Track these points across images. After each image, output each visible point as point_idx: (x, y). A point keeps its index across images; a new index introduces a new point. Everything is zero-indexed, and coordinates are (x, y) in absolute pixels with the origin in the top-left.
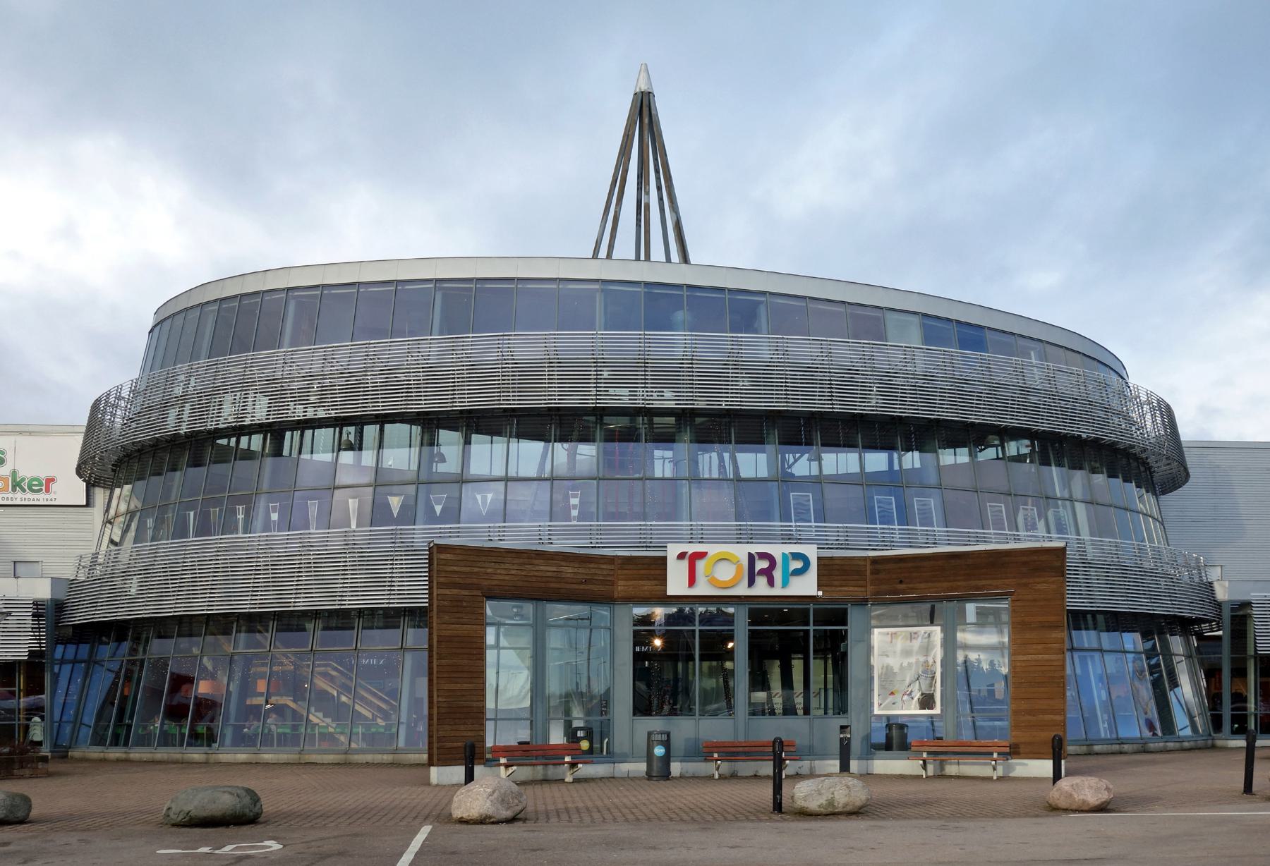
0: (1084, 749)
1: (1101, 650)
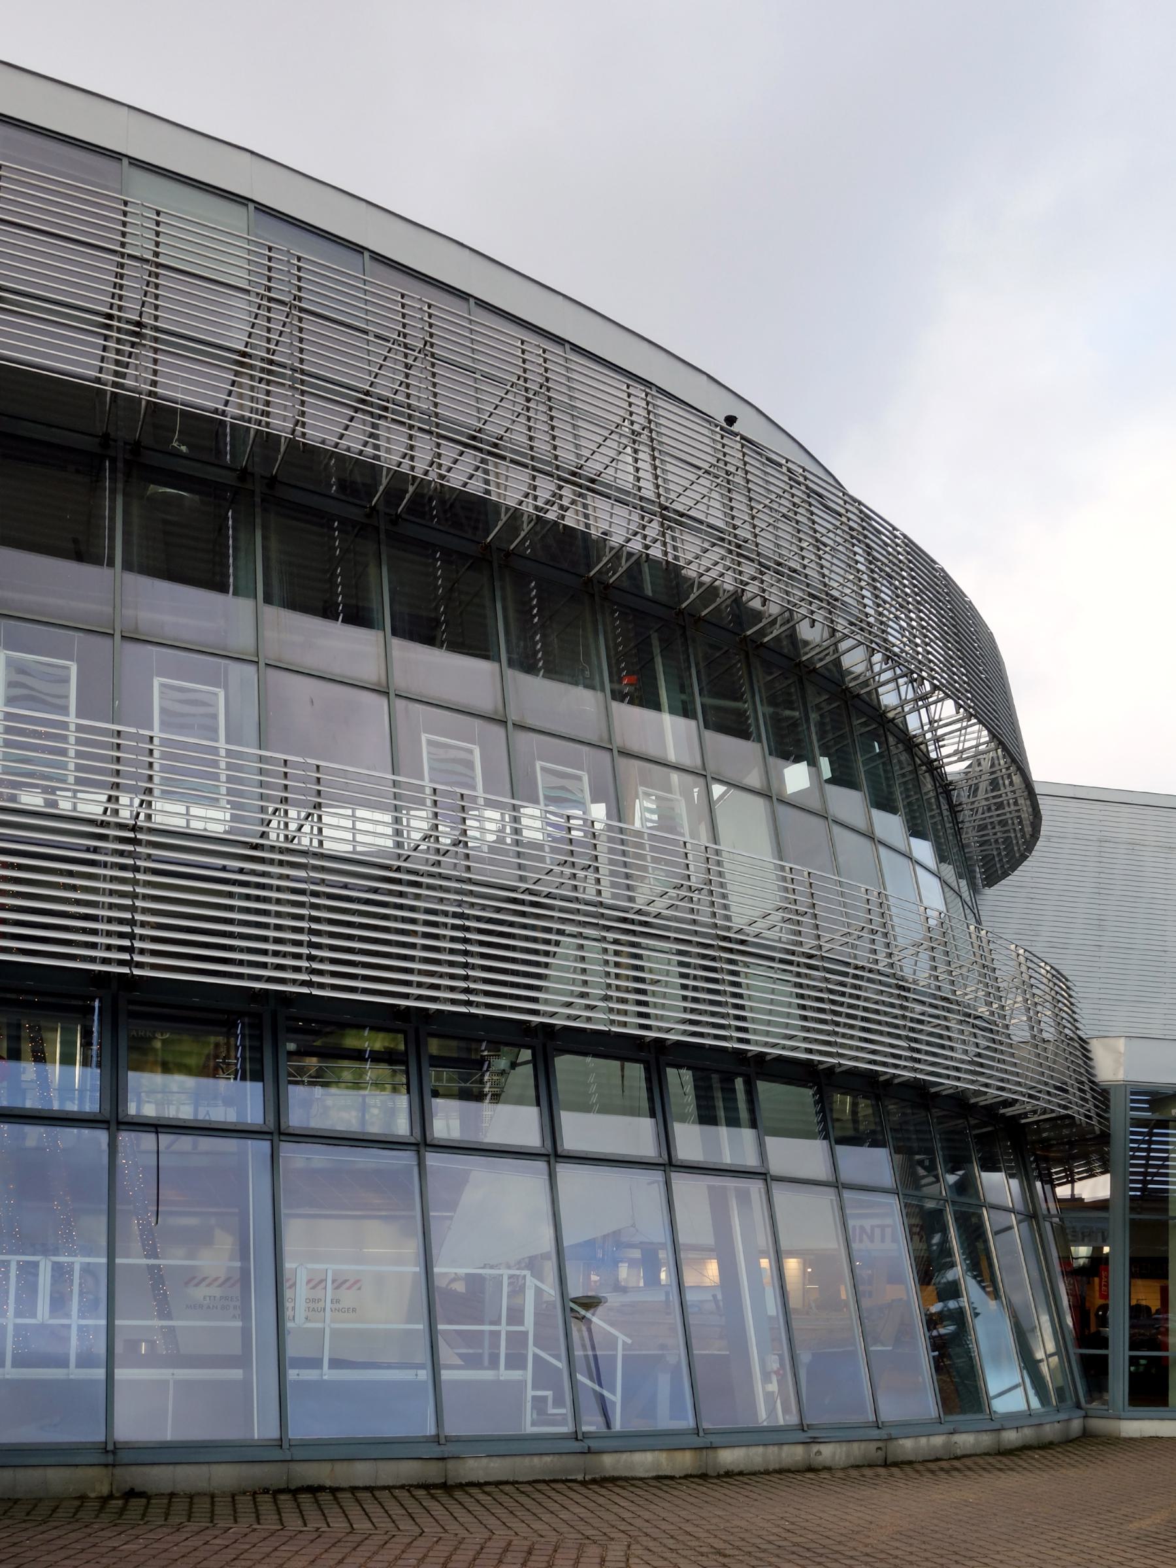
0: (685, 1461)
1: (763, 1175)
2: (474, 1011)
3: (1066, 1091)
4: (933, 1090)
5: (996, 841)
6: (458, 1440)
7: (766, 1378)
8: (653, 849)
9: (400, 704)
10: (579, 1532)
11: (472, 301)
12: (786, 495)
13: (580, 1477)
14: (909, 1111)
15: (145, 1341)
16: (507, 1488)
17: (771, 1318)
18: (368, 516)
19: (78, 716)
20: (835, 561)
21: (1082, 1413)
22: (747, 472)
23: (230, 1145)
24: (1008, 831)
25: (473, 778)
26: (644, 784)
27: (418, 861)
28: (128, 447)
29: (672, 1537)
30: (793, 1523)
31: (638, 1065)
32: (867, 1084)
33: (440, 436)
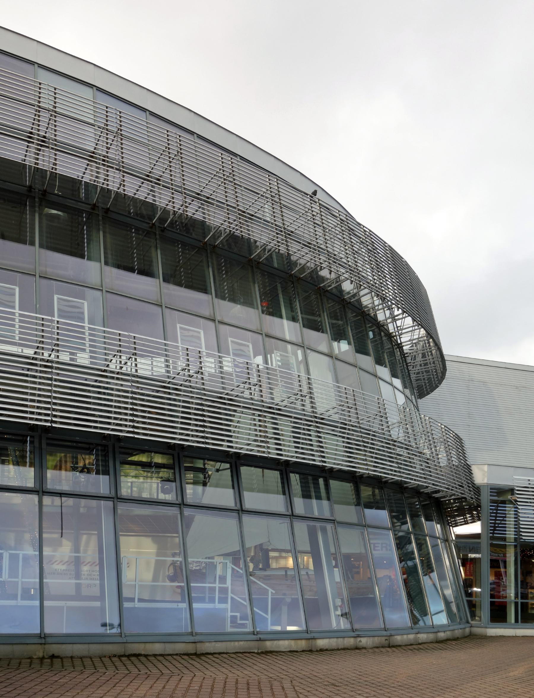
0: (302, 644)
2: (207, 446)
3: (463, 487)
4: (405, 485)
5: (424, 379)
6: (201, 634)
7: (336, 608)
8: (281, 377)
9: (167, 312)
10: (266, 675)
11: (195, 135)
12: (338, 226)
13: (256, 651)
14: (392, 494)
15: (33, 589)
16: (224, 655)
17: (337, 583)
18: (151, 228)
19: (19, 310)
20: (359, 258)
21: (469, 625)
22: (322, 215)
23: (94, 503)
24: (430, 375)
25: (201, 344)
26: (276, 350)
27: (179, 379)
28: (41, 192)
29: (309, 678)
30: (360, 672)
31: (276, 472)
32: (377, 482)
33: (124, 172)
